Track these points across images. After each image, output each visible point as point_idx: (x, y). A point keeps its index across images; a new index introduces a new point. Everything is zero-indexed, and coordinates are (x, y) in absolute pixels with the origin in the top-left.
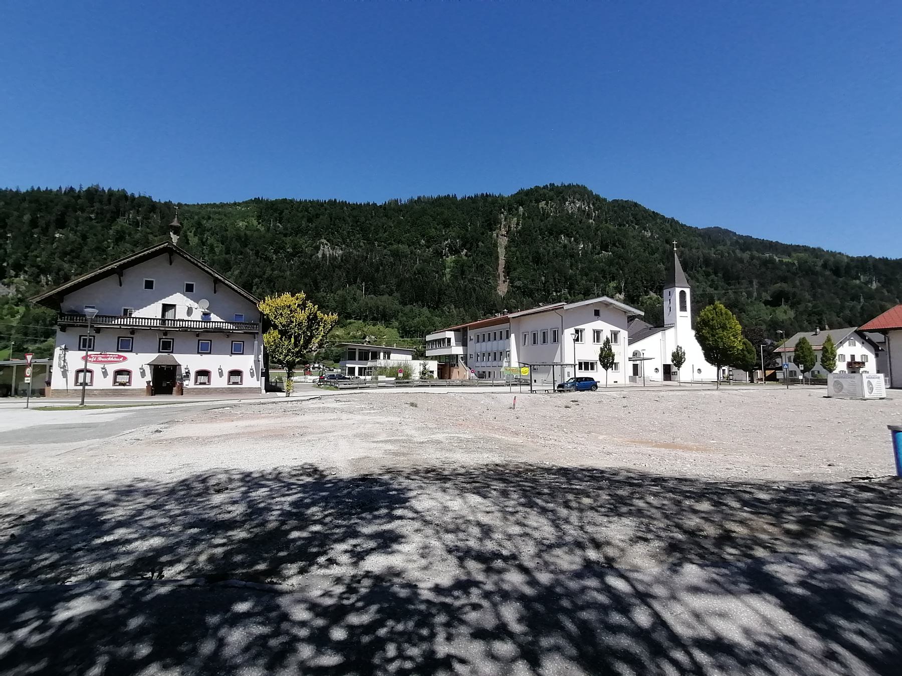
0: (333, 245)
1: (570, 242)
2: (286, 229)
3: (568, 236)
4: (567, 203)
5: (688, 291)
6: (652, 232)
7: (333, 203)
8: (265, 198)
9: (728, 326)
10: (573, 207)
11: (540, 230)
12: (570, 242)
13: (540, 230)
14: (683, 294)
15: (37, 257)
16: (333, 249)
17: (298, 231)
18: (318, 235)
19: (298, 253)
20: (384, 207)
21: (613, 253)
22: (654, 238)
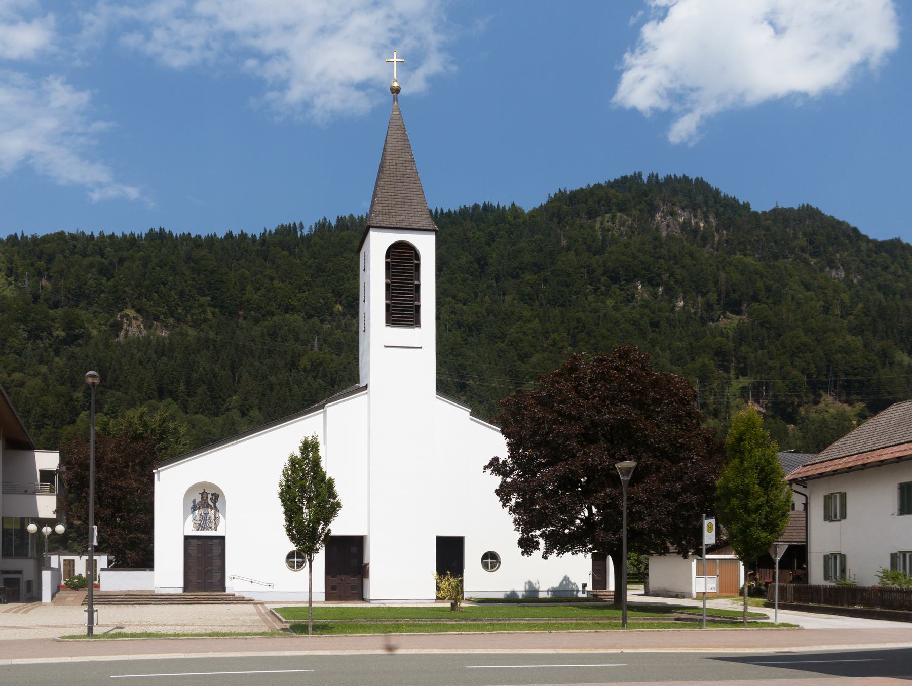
0: (150, 318)
1: (655, 295)
2: (57, 290)
3: (652, 282)
4: (658, 216)
5: (425, 245)
6: (848, 271)
7: (159, 238)
8: (29, 234)
9: (723, 414)
10: (668, 223)
11: (591, 272)
12: (655, 295)
13: (591, 272)
14: (402, 260)
15: (547, 434)
16: (149, 327)
17: (79, 296)
18: (118, 302)
19: (77, 337)
20: (266, 240)
21: (750, 315)
22: (850, 285)
